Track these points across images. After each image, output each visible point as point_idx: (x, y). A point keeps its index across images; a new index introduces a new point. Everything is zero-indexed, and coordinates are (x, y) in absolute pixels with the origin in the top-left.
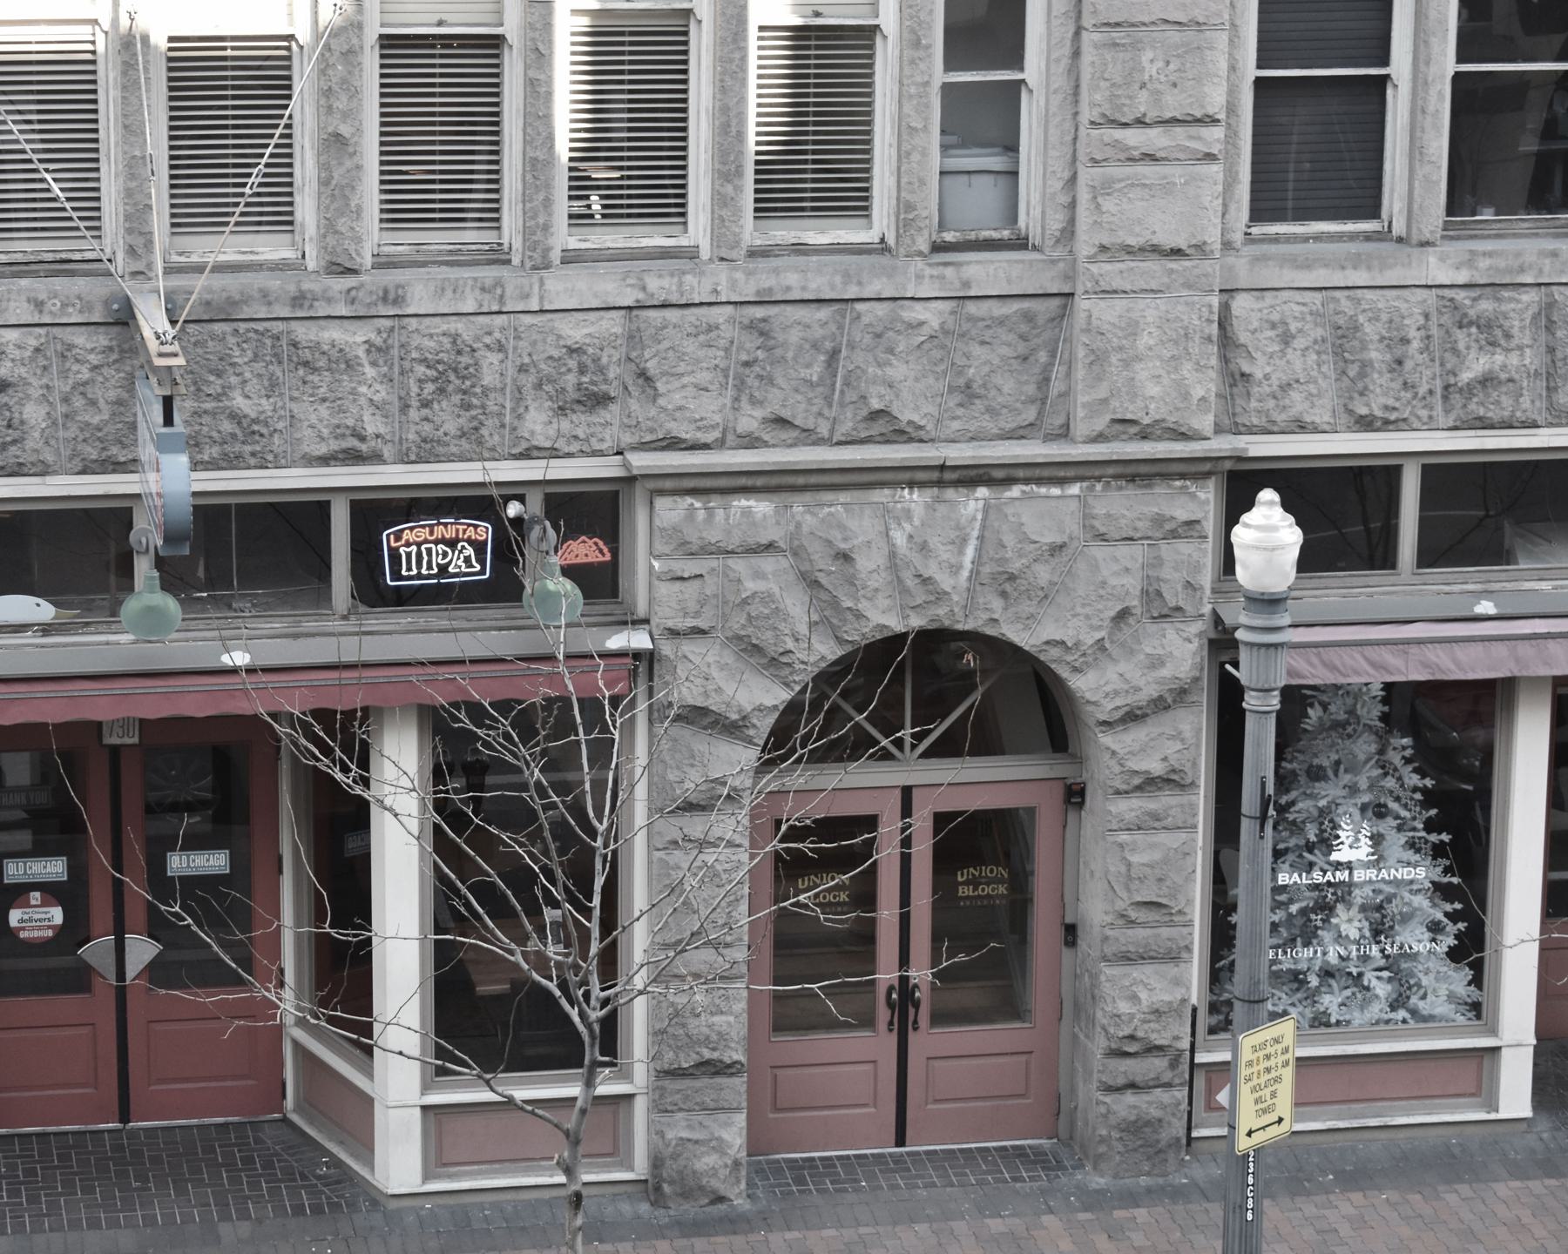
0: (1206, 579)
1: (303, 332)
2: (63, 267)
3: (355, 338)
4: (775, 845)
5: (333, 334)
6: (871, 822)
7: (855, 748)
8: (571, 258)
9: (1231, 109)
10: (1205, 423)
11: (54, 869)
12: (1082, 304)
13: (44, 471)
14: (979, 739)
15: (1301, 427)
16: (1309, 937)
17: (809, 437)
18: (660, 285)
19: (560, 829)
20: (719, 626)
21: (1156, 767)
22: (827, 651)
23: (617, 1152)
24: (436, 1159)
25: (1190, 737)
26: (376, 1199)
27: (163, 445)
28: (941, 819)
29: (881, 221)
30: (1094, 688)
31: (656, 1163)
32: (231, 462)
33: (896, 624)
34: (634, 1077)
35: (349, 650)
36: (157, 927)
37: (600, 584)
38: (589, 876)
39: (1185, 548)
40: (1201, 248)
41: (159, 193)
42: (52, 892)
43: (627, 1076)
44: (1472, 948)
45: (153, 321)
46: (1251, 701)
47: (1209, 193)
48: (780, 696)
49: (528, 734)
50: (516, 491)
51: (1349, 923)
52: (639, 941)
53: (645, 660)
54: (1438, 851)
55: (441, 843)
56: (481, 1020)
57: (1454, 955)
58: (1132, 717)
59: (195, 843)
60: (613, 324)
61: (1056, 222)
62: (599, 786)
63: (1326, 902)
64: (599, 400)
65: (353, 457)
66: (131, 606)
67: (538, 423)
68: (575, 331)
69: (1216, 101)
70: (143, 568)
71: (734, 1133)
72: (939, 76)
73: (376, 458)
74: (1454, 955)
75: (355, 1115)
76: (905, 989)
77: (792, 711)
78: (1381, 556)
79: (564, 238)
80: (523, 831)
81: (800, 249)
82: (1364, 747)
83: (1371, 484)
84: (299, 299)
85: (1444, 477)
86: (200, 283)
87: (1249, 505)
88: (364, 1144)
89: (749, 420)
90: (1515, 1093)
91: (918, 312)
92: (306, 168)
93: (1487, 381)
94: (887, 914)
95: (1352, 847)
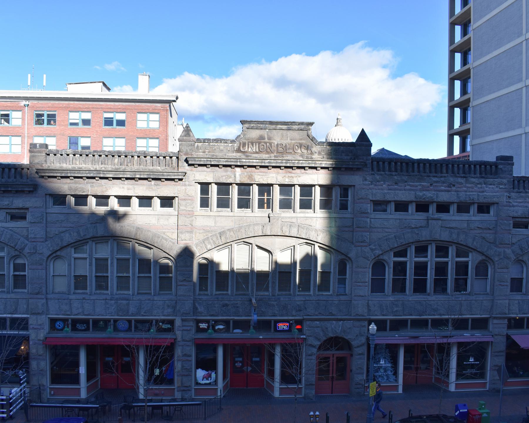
0: (366, 332)
1: (269, 302)
2: (245, 295)
3: (275, 303)
4: (319, 360)
5: (273, 302)
6: (329, 358)
7: (328, 349)
8: (298, 295)
9: (369, 281)
10: (366, 315)
11: (241, 359)
12: (353, 302)
13: (242, 316)
14: (341, 349)
15: (376, 315)
16: (377, 372)
17: (323, 315)
18: (307, 298)
19: (295, 357)
20: (313, 336)
21: (360, 352)
22: (325, 338)
23: (300, 393)
24: (281, 394)
25: (364, 349)
26: (274, 398)
27: (254, 314)
28: (337, 358)
29: (331, 292)
30: (354, 343)
31: (305, 395)
32: (261, 316)
33: (332, 336)
34: (302, 385)
35: (273, 337)
36: (251, 366)
37: (300, 330)
38: (298, 362)
39: (364, 328)
40: (365, 296)
41: (255, 287)
42: (240, 362)
43: (302, 385)
44: (396, 374)
45: (254, 301)
46: (371, 346)
47: (366, 290)
48: (319, 343)
49: (292, 347)
50: (292, 320)
51: (382, 371)
52: (304, 371)
53: (305, 339)
54: (392, 363)
55: (282, 359)
56: (286, 378)
57: (394, 374)
58: (358, 347)
59: (256, 357)
60: (302, 302)
61: (350, 293)
62: (300, 352)
63: (379, 368)
64: (300, 310)
65: (274, 316)
66: (250, 331)
67: (294, 313)
68: (298, 303)
69: (367, 280)
70: (251, 327)
71: (313, 392)
72: (337, 277)
73: (277, 316)
74: (394, 374)
75: (272, 388)
76: (333, 377)
77: (321, 344)
78: (385, 330)
79: (297, 293)
80: (291, 359)
81: (323, 295)
82: (383, 351)
83: (384, 322)
84: (269, 299)
85: (392, 321)
86: (259, 297)
87: (371, 324)
88: (273, 391)
89: (316, 313)
90: (400, 391)
91: (335, 302)
92: (270, 285)
93: (396, 311)
94: (331, 368)
95: (382, 362)
